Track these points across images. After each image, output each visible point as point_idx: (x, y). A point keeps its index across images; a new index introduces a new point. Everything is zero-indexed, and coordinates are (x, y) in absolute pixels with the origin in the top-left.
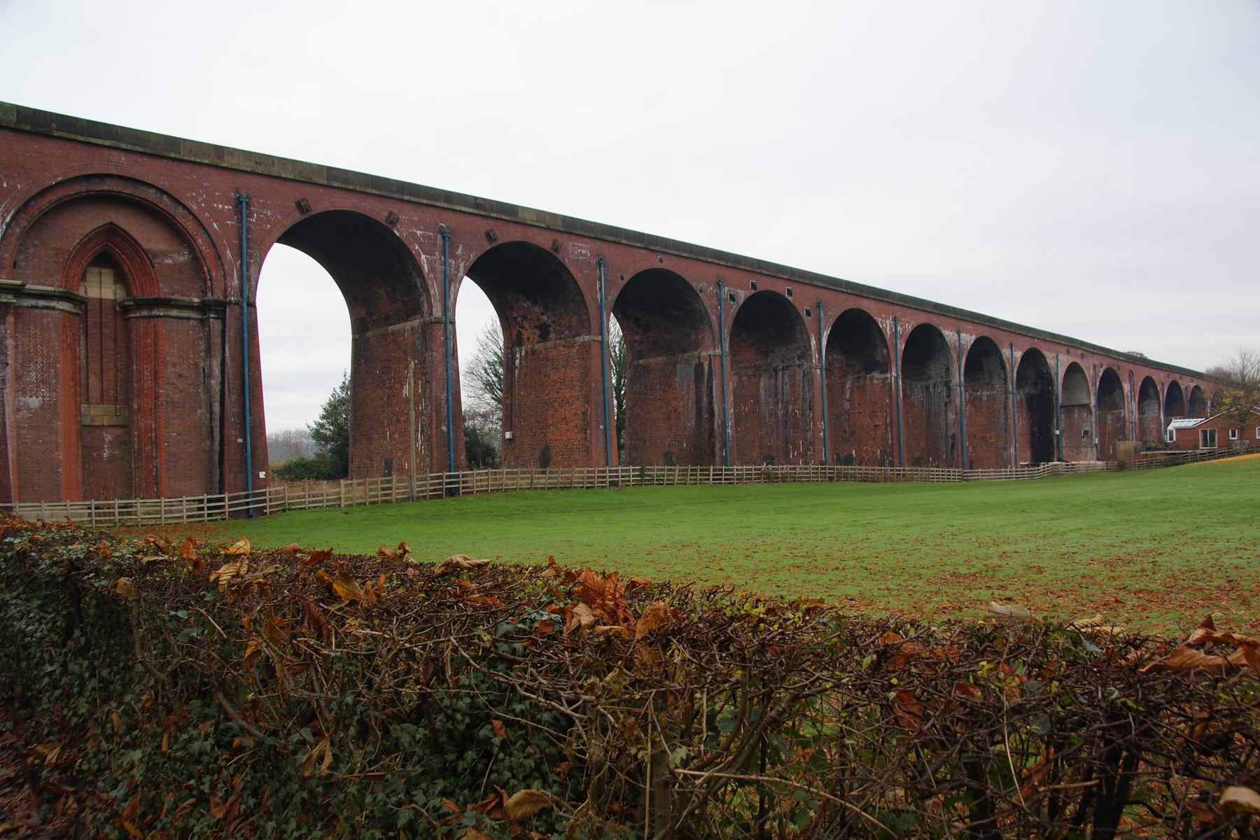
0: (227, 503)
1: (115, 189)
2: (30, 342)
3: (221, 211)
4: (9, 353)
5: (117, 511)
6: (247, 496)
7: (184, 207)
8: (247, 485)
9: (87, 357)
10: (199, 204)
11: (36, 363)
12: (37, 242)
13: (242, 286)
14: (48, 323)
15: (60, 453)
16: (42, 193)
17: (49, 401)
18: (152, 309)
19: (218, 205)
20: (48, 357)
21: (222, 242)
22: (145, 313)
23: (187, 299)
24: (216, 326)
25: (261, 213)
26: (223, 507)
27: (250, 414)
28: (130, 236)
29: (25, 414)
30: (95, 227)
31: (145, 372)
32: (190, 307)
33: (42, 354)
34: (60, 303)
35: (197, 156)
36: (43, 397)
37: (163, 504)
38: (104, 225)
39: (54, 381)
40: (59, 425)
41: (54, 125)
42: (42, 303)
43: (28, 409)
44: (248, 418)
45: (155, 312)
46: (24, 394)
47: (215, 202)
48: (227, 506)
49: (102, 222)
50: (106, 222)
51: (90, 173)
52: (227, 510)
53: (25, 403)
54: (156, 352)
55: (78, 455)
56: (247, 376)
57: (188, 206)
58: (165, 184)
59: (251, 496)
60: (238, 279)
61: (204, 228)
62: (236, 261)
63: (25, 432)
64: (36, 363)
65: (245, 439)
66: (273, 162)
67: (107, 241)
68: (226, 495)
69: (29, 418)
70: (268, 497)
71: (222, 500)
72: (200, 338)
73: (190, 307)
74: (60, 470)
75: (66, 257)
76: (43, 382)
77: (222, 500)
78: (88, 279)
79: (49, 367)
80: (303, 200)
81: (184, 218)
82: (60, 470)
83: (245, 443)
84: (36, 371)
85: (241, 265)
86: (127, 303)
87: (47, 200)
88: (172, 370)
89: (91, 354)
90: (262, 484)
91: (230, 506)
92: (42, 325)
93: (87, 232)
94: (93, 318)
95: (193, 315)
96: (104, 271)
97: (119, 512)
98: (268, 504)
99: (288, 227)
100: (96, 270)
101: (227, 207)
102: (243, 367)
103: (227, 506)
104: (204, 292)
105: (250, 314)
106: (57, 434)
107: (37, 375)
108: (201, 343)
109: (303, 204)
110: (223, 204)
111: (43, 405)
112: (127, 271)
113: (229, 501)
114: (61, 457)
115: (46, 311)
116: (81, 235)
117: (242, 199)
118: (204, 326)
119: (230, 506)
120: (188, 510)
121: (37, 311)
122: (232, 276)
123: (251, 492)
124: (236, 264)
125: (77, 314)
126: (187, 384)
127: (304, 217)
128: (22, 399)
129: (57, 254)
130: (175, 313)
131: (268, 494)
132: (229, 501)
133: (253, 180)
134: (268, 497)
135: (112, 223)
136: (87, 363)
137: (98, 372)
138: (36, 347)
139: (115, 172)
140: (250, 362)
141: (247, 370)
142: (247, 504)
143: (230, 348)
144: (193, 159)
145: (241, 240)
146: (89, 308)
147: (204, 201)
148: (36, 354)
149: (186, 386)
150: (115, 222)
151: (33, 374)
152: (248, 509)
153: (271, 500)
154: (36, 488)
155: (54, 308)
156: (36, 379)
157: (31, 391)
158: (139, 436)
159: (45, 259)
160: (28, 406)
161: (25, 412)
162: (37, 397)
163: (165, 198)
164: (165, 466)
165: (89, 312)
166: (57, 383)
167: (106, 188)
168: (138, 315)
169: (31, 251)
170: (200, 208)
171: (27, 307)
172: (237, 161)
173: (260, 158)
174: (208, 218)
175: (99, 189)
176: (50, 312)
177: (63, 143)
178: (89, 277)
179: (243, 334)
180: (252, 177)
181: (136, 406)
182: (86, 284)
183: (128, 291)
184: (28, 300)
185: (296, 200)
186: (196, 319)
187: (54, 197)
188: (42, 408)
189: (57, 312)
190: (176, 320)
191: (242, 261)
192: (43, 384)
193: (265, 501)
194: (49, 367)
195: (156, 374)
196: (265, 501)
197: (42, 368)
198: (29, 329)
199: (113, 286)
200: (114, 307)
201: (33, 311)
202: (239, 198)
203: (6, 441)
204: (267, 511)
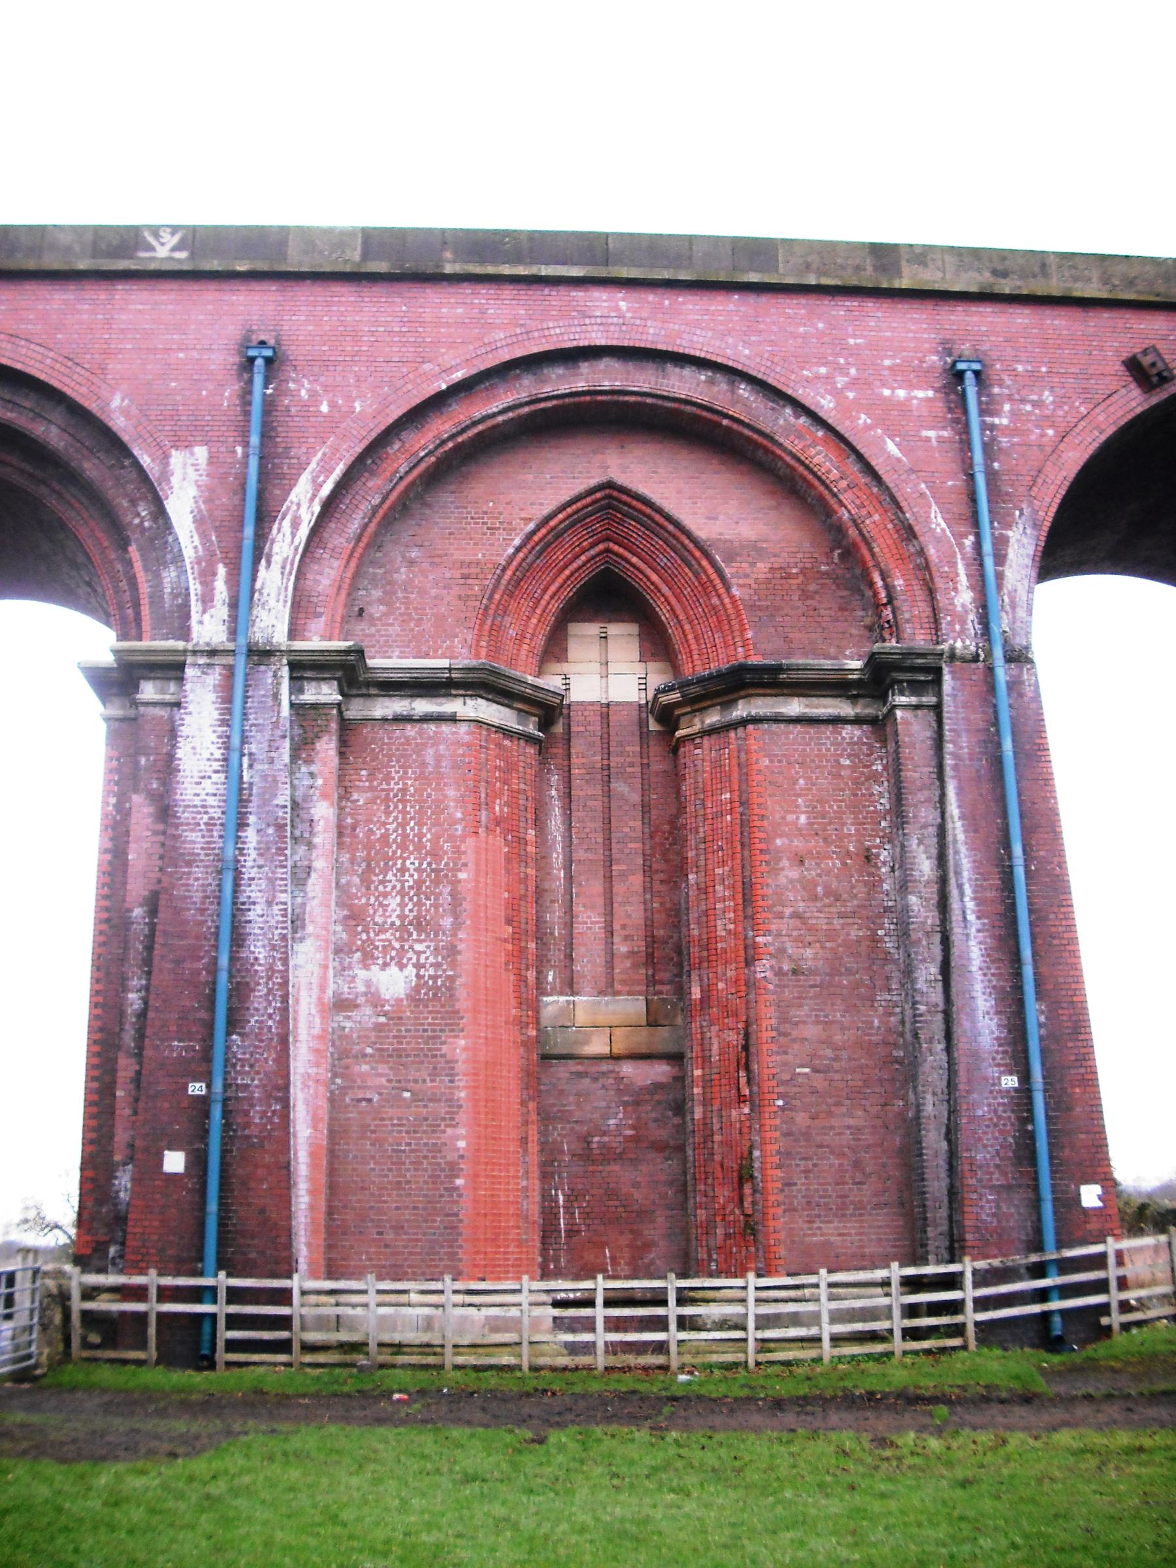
0: (969, 1293)
1: (606, 385)
2: (388, 813)
3: (903, 407)
4: (317, 840)
5: (600, 1312)
6: (1039, 1271)
7: (800, 408)
8: (1038, 1230)
9: (568, 866)
10: (837, 394)
11: (403, 870)
12: (414, 554)
13: (984, 606)
14: (438, 758)
15: (462, 1131)
16: (417, 415)
17: (434, 978)
18: (729, 704)
19: (893, 389)
20: (435, 854)
21: (908, 489)
22: (713, 718)
23: (827, 664)
24: (916, 728)
25: (1023, 401)
26: (955, 1307)
27: (1039, 995)
28: (659, 510)
29: (366, 1016)
30: (566, 497)
31: (719, 888)
32: (838, 686)
33: (419, 846)
34: (470, 702)
35: (821, 273)
36: (418, 966)
37: (752, 1295)
38: (590, 492)
39: (447, 922)
40: (459, 1047)
41: (448, 255)
42: (422, 706)
43: (375, 1001)
44: (1034, 1011)
45: (741, 710)
46: (367, 959)
47: (884, 385)
48: (969, 1305)
49: (581, 486)
50: (593, 482)
51: (535, 350)
52: (971, 1317)
53: (368, 983)
54: (745, 824)
55: (524, 1141)
56: (1020, 872)
57: (807, 402)
58: (739, 354)
59: (1053, 1269)
60: (972, 587)
61: (860, 457)
62: (960, 536)
63: (365, 1068)
64: (403, 870)
65: (1025, 1077)
66: (1043, 266)
67: (608, 539)
68: (967, 1267)
69: (379, 1027)
70: (1112, 1272)
71: (951, 1282)
72: (875, 777)
73: (838, 686)
74: (459, 1182)
75: (489, 582)
76: (420, 924)
77: (951, 1282)
78: (571, 655)
79: (436, 882)
80: (1145, 352)
81: (800, 437)
82: (459, 1182)
83: (1025, 1091)
84: (402, 893)
85: (978, 546)
86: (664, 699)
87: (431, 435)
88: (794, 874)
89: (579, 854)
90: (1093, 1226)
91: (982, 1304)
92: (423, 764)
93: (546, 511)
94: (585, 754)
95: (844, 708)
96: (614, 629)
97: (607, 1319)
98: (1115, 1296)
99: (1110, 431)
100: (592, 629)
101: (920, 394)
102: (1007, 844)
103: (969, 1305)
104: (877, 630)
105: (1014, 685)
106: (452, 1076)
107: (402, 905)
108: (876, 789)
109: (1146, 361)
110: (910, 386)
111: (417, 989)
112: (664, 614)
113: (976, 1285)
114: (462, 1144)
115: (432, 728)
116: (527, 520)
117: (961, 366)
118: (884, 742)
119: (982, 1304)
120: (836, 1317)
121: (410, 730)
122: (953, 579)
123: (1051, 1255)
124: (961, 546)
125: (529, 739)
126: (841, 916)
127: (1155, 400)
128: (362, 974)
129: (466, 577)
130: (795, 707)
131: (1111, 1260)
132: (976, 1285)
133: (984, 318)
134: (1112, 1272)
135: (610, 485)
136: (570, 878)
137: (600, 901)
138: (403, 825)
139: (602, 341)
140: (1027, 833)
141: (1017, 849)
142: (1042, 1295)
143: (960, 792)
144: (812, 280)
145: (971, 477)
146: (574, 729)
147: (853, 383)
148: (403, 846)
149: (837, 923)
150: (621, 479)
151: (393, 902)
152: (1046, 1316)
153: (1123, 1284)
154: (389, 1236)
155: (452, 719)
156: (402, 917)
157: (387, 948)
158: (707, 1083)
159: (434, 592)
160: (377, 992)
161: (368, 1011)
162: (402, 967)
163: (744, 390)
164: (779, 1173)
165: (573, 742)
166: (457, 926)
167: (581, 385)
168: (697, 727)
169: (402, 575)
170: (844, 408)
171: (385, 720)
172: (940, 275)
173: (1004, 259)
174: (868, 428)
175: (564, 389)
176: (446, 728)
177: (467, 289)
178: (575, 649)
179: (999, 745)
180: (987, 309)
181: (696, 993)
182: (565, 667)
183: (675, 668)
184: (387, 702)
185: (1125, 355)
186: (857, 721)
187: (441, 427)
188: (414, 998)
189: (463, 728)
190: (799, 728)
191: (978, 536)
192: (420, 928)
193: (1101, 1286)
194: (436, 882)
195: (748, 895)
196: (1101, 1286)
197: (419, 883)
198: (388, 778)
199: (639, 668)
200: (642, 724)
201: (397, 731)
202: (954, 363)
203: (286, 1087)
204: (1115, 1319)
